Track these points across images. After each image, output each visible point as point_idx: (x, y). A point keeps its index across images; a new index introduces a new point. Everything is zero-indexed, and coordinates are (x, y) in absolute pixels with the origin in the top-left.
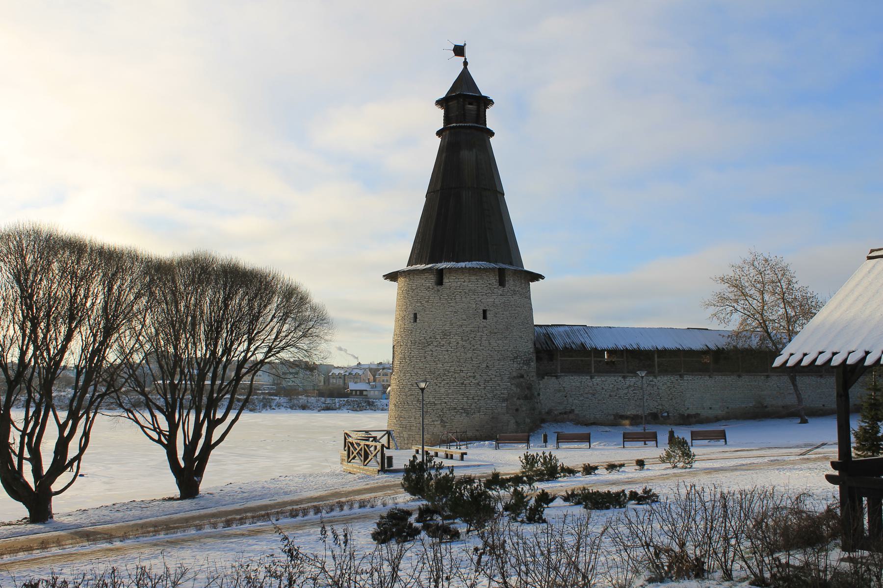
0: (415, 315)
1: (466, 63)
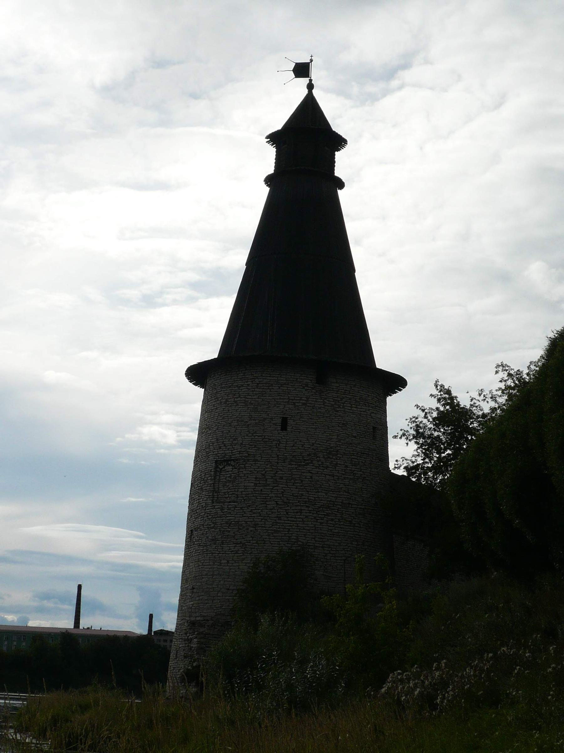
0: (284, 421)
1: (310, 87)
